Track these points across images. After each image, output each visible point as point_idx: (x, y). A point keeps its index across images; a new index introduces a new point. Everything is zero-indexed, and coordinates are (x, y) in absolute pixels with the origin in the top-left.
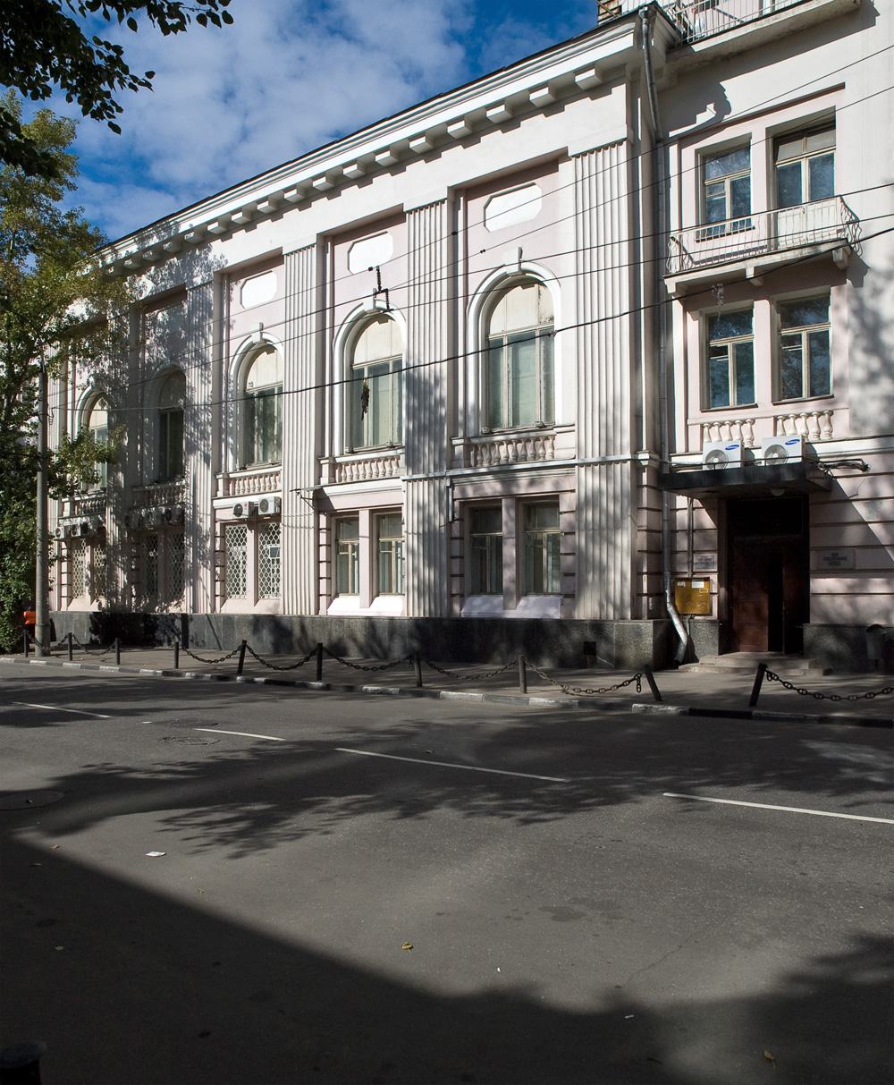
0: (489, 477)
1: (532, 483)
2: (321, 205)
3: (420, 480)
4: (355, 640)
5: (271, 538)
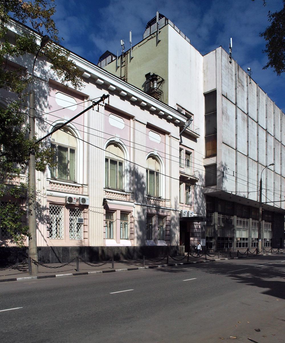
0: (154, 208)
1: (162, 212)
2: (155, 117)
3: (139, 205)
4: (122, 254)
5: (76, 214)
